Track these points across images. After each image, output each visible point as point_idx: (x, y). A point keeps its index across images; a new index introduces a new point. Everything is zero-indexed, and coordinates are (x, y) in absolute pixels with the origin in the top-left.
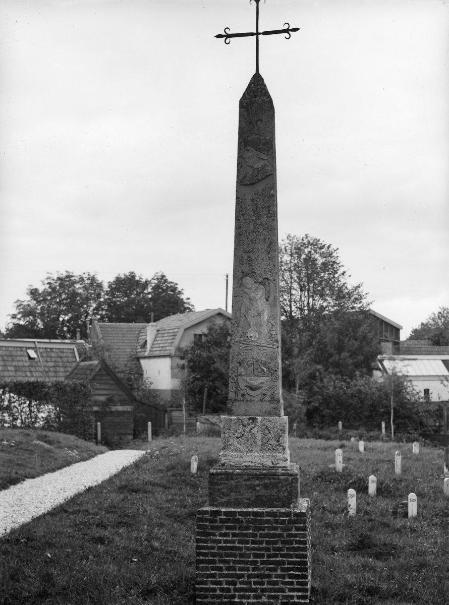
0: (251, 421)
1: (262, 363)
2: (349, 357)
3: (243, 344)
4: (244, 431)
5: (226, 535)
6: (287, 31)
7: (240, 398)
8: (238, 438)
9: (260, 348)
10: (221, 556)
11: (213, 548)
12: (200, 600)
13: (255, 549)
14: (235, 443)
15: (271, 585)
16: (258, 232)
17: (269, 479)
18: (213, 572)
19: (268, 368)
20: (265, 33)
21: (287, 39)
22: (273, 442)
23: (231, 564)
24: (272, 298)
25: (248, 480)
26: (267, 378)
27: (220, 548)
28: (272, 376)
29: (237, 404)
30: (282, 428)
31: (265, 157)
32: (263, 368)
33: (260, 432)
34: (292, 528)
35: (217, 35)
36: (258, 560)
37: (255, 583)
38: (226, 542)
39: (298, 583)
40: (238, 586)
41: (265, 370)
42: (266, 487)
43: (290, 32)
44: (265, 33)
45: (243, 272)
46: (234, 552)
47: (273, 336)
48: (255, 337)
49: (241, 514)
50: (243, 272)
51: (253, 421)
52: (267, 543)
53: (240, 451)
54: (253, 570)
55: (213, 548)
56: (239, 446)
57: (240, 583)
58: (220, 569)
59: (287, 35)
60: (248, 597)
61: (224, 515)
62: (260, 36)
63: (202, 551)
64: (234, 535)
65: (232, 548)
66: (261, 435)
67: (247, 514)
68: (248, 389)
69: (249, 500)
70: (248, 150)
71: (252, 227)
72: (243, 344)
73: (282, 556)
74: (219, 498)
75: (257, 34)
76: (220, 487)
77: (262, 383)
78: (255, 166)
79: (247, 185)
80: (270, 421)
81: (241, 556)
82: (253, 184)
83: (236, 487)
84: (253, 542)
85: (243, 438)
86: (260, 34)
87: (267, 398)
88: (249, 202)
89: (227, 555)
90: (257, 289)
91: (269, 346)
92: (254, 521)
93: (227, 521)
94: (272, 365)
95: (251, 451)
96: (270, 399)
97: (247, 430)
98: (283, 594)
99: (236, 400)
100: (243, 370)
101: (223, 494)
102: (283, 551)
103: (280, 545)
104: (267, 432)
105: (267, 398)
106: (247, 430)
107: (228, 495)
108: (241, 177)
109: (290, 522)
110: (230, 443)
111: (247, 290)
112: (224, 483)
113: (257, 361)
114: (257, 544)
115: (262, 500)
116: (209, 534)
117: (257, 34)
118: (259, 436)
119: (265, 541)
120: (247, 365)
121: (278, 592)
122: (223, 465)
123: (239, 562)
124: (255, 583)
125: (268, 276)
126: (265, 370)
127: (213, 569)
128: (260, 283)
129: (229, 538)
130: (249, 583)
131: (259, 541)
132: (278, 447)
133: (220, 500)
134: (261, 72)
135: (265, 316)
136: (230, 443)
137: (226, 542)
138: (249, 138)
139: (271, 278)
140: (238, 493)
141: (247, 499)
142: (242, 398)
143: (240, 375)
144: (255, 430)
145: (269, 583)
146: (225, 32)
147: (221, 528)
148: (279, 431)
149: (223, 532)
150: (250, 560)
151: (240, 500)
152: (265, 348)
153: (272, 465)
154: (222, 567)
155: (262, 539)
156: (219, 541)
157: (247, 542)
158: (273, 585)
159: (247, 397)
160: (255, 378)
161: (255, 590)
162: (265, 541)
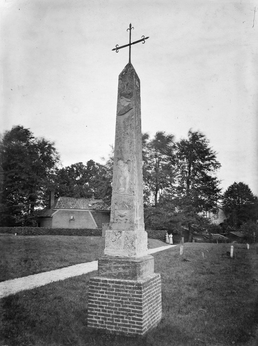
0: (119, 233)
1: (126, 203)
2: (55, 172)
3: (117, 194)
4: (116, 238)
5: (102, 292)
6: (143, 40)
7: (115, 221)
8: (113, 242)
9: (125, 195)
10: (99, 303)
11: (96, 299)
12: (89, 326)
13: (116, 301)
14: (112, 245)
15: (123, 322)
16: (126, 138)
17: (125, 264)
18: (96, 312)
19: (129, 206)
20: (134, 43)
21: (143, 43)
22: (130, 244)
23: (104, 309)
24: (131, 170)
25: (115, 264)
26: (128, 211)
27: (99, 299)
28: (130, 210)
29: (113, 224)
30: (134, 237)
31: (130, 100)
32: (126, 206)
33: (123, 239)
34: (135, 291)
35: (113, 49)
36: (117, 308)
37: (116, 320)
38: (102, 296)
39: (137, 323)
40: (107, 321)
41: (127, 207)
42: (124, 268)
43: (145, 40)
44: (134, 43)
45: (118, 158)
46: (106, 302)
47: (131, 189)
48: (123, 190)
49: (110, 282)
50: (118, 158)
51: (120, 233)
52: (122, 299)
53: (114, 248)
54: (115, 313)
55: (96, 299)
56: (113, 246)
57: (108, 319)
58: (99, 310)
59: (143, 42)
60: (112, 328)
61: (102, 282)
62: (132, 46)
63: (91, 300)
64: (106, 293)
65: (105, 300)
66: (124, 240)
67: (113, 282)
68: (119, 216)
69: (116, 275)
70: (122, 98)
71: (123, 136)
72: (117, 194)
73: (130, 307)
74: (101, 273)
75: (130, 45)
76: (102, 267)
77: (125, 213)
78: (125, 106)
79: (121, 115)
80: (128, 233)
81: (109, 304)
82: (124, 114)
83: (109, 267)
84: (115, 298)
85: (115, 242)
86: (132, 44)
87: (128, 221)
88: (122, 123)
89: (103, 303)
90: (124, 166)
91: (130, 194)
92: (116, 286)
93: (103, 285)
94: (130, 204)
95: (119, 249)
96: (129, 222)
97: (117, 237)
98: (129, 328)
99: (113, 222)
100: (117, 207)
101: (104, 271)
102: (130, 304)
103: (128, 301)
104: (127, 239)
105: (128, 221)
106: (117, 237)
107: (106, 271)
108: (119, 112)
109: (134, 288)
110: (109, 244)
111: (119, 167)
112: (104, 265)
113: (124, 202)
114: (117, 299)
115: (122, 275)
116: (94, 292)
117: (130, 45)
118: (123, 241)
119: (121, 298)
120: (119, 204)
121: (127, 327)
122: (106, 255)
123: (108, 308)
124: (116, 320)
125: (130, 159)
126: (127, 207)
127: (96, 310)
128: (126, 163)
129: (104, 294)
130: (112, 320)
131: (118, 297)
132: (132, 247)
133: (102, 274)
134: (132, 63)
135: (128, 179)
136: (109, 244)
137: (102, 296)
138: (122, 92)
139: (131, 160)
140: (110, 271)
141: (114, 274)
142: (116, 221)
143: (116, 209)
144: (121, 238)
145: (123, 321)
146: (116, 47)
147: (100, 288)
148: (133, 239)
149: (101, 291)
150: (113, 307)
151: (111, 274)
152: (127, 196)
153: (128, 257)
154: (100, 310)
155: (120, 297)
156: (99, 296)
157: (112, 297)
158: (125, 322)
159: (119, 221)
160: (122, 211)
161: (116, 324)
162: (121, 298)
